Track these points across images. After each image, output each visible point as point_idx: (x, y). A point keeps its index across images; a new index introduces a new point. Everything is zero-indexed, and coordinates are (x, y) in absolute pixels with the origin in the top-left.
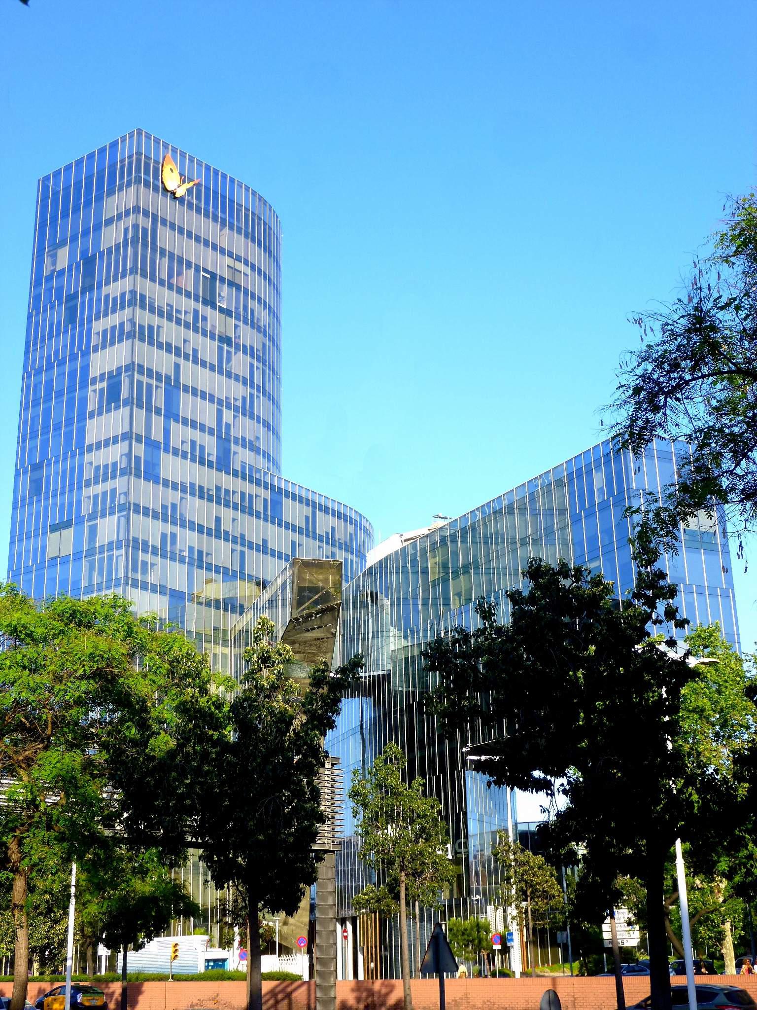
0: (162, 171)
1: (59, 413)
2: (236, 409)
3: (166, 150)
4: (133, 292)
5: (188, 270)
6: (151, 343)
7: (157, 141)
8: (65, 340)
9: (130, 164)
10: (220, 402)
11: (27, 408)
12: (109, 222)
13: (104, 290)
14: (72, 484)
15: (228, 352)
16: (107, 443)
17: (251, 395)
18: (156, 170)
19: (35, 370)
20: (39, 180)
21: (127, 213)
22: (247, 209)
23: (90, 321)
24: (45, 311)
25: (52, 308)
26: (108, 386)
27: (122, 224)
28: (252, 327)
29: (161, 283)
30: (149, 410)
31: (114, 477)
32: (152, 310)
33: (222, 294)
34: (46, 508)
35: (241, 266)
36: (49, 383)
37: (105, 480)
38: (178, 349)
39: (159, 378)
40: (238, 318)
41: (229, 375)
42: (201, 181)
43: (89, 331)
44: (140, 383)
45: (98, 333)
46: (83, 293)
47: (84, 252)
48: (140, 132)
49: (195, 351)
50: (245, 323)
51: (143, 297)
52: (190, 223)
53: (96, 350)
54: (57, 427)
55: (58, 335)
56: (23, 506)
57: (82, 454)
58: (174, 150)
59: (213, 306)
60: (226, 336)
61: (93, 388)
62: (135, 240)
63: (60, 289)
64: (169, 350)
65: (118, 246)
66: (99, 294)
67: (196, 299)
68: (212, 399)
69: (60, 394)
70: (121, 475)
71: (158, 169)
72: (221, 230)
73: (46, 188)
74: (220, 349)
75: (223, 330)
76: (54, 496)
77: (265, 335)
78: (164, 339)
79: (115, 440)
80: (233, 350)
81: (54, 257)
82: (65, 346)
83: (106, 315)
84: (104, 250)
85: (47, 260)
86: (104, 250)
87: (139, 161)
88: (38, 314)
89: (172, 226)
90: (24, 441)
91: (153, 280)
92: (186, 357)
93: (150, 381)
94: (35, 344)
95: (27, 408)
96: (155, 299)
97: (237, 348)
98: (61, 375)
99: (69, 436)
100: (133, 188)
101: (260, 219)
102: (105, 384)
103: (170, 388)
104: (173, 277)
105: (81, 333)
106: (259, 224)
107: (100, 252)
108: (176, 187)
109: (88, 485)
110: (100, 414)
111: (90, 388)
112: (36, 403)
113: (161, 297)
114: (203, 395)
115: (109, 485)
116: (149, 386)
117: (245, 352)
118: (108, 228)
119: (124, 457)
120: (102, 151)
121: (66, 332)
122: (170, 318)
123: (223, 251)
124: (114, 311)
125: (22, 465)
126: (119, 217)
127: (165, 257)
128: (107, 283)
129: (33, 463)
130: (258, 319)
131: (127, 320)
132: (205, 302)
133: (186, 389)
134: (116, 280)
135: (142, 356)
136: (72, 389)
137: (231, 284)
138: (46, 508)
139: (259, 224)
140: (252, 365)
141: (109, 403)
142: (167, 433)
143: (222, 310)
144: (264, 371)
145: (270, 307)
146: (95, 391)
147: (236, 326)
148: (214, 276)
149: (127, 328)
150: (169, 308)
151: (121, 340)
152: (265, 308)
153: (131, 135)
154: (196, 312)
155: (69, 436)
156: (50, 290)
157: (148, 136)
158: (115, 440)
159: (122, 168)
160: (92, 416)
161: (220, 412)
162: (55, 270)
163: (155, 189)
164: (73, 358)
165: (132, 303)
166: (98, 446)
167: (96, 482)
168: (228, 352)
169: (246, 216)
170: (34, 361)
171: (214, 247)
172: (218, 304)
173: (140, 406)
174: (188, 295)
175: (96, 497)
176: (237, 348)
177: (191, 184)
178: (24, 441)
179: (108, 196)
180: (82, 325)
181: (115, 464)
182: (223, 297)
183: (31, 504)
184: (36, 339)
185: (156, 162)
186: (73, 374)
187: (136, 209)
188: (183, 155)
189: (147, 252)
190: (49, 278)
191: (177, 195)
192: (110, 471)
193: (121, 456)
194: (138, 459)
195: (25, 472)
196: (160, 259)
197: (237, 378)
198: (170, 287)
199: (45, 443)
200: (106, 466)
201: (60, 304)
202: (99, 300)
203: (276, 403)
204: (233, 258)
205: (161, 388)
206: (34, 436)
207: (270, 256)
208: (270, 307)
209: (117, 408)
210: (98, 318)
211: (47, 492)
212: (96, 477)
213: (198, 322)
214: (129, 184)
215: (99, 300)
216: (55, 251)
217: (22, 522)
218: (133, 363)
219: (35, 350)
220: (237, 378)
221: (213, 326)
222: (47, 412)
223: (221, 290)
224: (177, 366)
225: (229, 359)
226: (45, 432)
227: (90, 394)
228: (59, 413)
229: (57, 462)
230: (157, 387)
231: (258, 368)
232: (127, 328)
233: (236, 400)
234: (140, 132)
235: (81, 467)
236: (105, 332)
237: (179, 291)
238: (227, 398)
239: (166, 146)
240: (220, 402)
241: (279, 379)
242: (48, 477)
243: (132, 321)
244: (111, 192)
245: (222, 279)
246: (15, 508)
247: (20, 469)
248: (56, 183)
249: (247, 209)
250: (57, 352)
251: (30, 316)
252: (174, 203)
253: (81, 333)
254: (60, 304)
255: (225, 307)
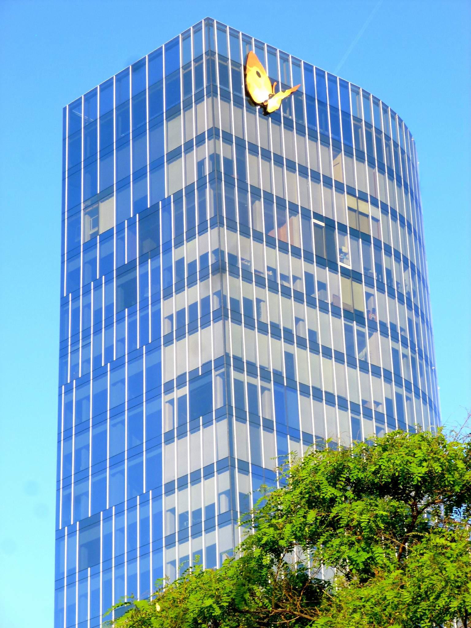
0: (245, 75)
1: (118, 439)
2: (379, 418)
3: (247, 47)
4: (218, 253)
5: (293, 217)
6: (250, 325)
7: (234, 34)
8: (120, 331)
9: (199, 70)
10: (355, 408)
11: (68, 438)
12: (175, 155)
13: (175, 254)
14: (145, 545)
15: (361, 335)
16: (196, 478)
17: (399, 397)
18: (236, 75)
19: (77, 379)
20: (65, 109)
21: (200, 140)
22: (369, 125)
23: (156, 301)
24: (87, 292)
25: (98, 287)
26: (190, 392)
27: (194, 156)
28: (391, 294)
29: (258, 237)
30: (255, 423)
31: (210, 528)
32: (247, 278)
33: (344, 249)
34: (107, 584)
35: (367, 208)
36: (100, 397)
37: (197, 534)
38: (288, 333)
39: (265, 376)
40: (369, 284)
41: (364, 367)
42: (301, 86)
43: (157, 315)
44: (239, 384)
45: (170, 318)
46: (143, 262)
47: (140, 204)
48: (209, 23)
49: (313, 334)
50: (381, 289)
51: (233, 258)
52: (291, 149)
53: (169, 341)
54: (117, 461)
55: (109, 325)
56: (71, 584)
57: (157, 497)
58: (260, 46)
59: (333, 267)
60: (355, 310)
61: (169, 397)
62: (215, 178)
63: (107, 260)
64: (276, 334)
65: (190, 189)
66: (167, 261)
67: (308, 258)
68: (343, 404)
69: (117, 412)
70: (221, 525)
71: (239, 73)
72: (335, 157)
73: (75, 120)
74: (349, 330)
75: (349, 302)
76: (120, 564)
77: (409, 307)
78: (267, 319)
79: (209, 472)
80: (366, 330)
81: (94, 214)
82: (121, 341)
83: (180, 289)
84: (169, 197)
85: (84, 220)
86: (169, 197)
87: (211, 64)
88: (76, 298)
89: (266, 155)
90: (67, 486)
91: (245, 233)
92: (301, 344)
93: (253, 381)
94: (75, 342)
95: (68, 438)
96: (250, 262)
97: (373, 328)
98: (118, 383)
99: (135, 472)
100: (206, 103)
101: (388, 138)
102: (186, 390)
103: (282, 390)
104: (272, 228)
105: (144, 319)
106: (388, 145)
107: (164, 200)
108: (267, 98)
109: (170, 543)
110: (182, 434)
111: (164, 398)
112: (82, 429)
113: (259, 258)
114: (330, 399)
115: (204, 541)
116: (252, 388)
117: (384, 333)
118: (175, 164)
119: (223, 497)
120: (155, 56)
121: (121, 320)
122: (273, 288)
123: (340, 187)
124: (192, 283)
125: (66, 522)
126: (189, 147)
127: (260, 200)
128: (179, 243)
129: (82, 518)
130: (398, 283)
131: (214, 294)
132: (321, 263)
133: (305, 390)
134: (190, 237)
135: (238, 342)
136: (135, 403)
137: (356, 234)
138: (107, 584)
139: (388, 145)
140: (395, 352)
141: (194, 418)
142: (283, 454)
143: (345, 273)
144: (413, 360)
145: (412, 265)
146: (171, 402)
147: (368, 295)
148: (330, 223)
149: (214, 305)
150: (271, 273)
151: (205, 324)
152: (406, 268)
153: (197, 29)
154: (309, 277)
155: (135, 472)
156: (93, 262)
157: (222, 29)
158: (209, 472)
159: (187, 76)
160: (169, 439)
161: (356, 424)
162: (98, 231)
163: (238, 103)
164: (135, 356)
165: (219, 269)
166: (183, 483)
167: (183, 539)
168: (361, 335)
169: (369, 135)
170: (75, 367)
171: (328, 182)
172: (340, 264)
173: (241, 418)
174: (296, 252)
175: (184, 560)
176: (373, 328)
177: (288, 93)
178: (67, 486)
179: (169, 118)
180: (144, 307)
181: (210, 509)
182: (346, 254)
183: (83, 579)
184: (75, 334)
185: (236, 64)
186: (136, 380)
187: (214, 133)
188: (272, 52)
189: (233, 194)
190: (90, 246)
191: (270, 110)
192: (203, 519)
193: (219, 495)
194: (244, 498)
195: (72, 533)
196: (253, 203)
197: (376, 371)
198: (271, 243)
199: (99, 488)
200: (197, 514)
201: (109, 281)
202: (168, 269)
203: (433, 407)
204: (355, 196)
205: (269, 390)
206: (82, 477)
207: (410, 233)
208: (413, 265)
209: (208, 423)
210: (168, 295)
211: (107, 560)
212: (183, 531)
213: (313, 292)
214: (199, 98)
215: (168, 269)
216: (95, 206)
217: (71, 609)
218: (227, 355)
219: (75, 352)
220: (376, 371)
221: (336, 297)
222: (100, 439)
223: (342, 244)
224: (289, 357)
225: (362, 345)
226: (99, 468)
227: (165, 409)
228: (118, 439)
229: (120, 513)
230: (263, 389)
231: (404, 356)
232: (214, 305)
233: (377, 404)
234: (209, 23)
235: (158, 517)
236: (181, 314)
237: (284, 248)
238: (364, 402)
239: (247, 41)
240: (355, 408)
241: (434, 371)
242: (107, 538)
243: (220, 295)
244: (173, 113)
245: (343, 228)
246: (59, 588)
247: (63, 528)
248: (91, 110)
249: (369, 125)
250: (109, 350)
251: (64, 302)
252: (265, 121)
253: (144, 319)
254: (109, 281)
255: (350, 268)
